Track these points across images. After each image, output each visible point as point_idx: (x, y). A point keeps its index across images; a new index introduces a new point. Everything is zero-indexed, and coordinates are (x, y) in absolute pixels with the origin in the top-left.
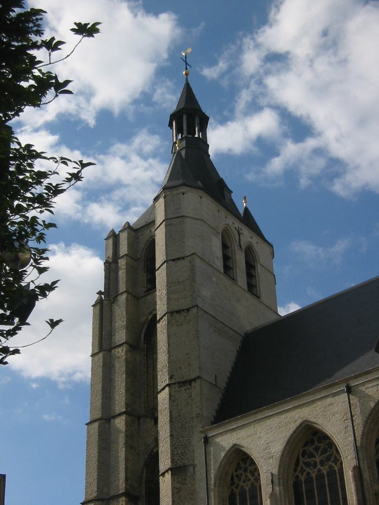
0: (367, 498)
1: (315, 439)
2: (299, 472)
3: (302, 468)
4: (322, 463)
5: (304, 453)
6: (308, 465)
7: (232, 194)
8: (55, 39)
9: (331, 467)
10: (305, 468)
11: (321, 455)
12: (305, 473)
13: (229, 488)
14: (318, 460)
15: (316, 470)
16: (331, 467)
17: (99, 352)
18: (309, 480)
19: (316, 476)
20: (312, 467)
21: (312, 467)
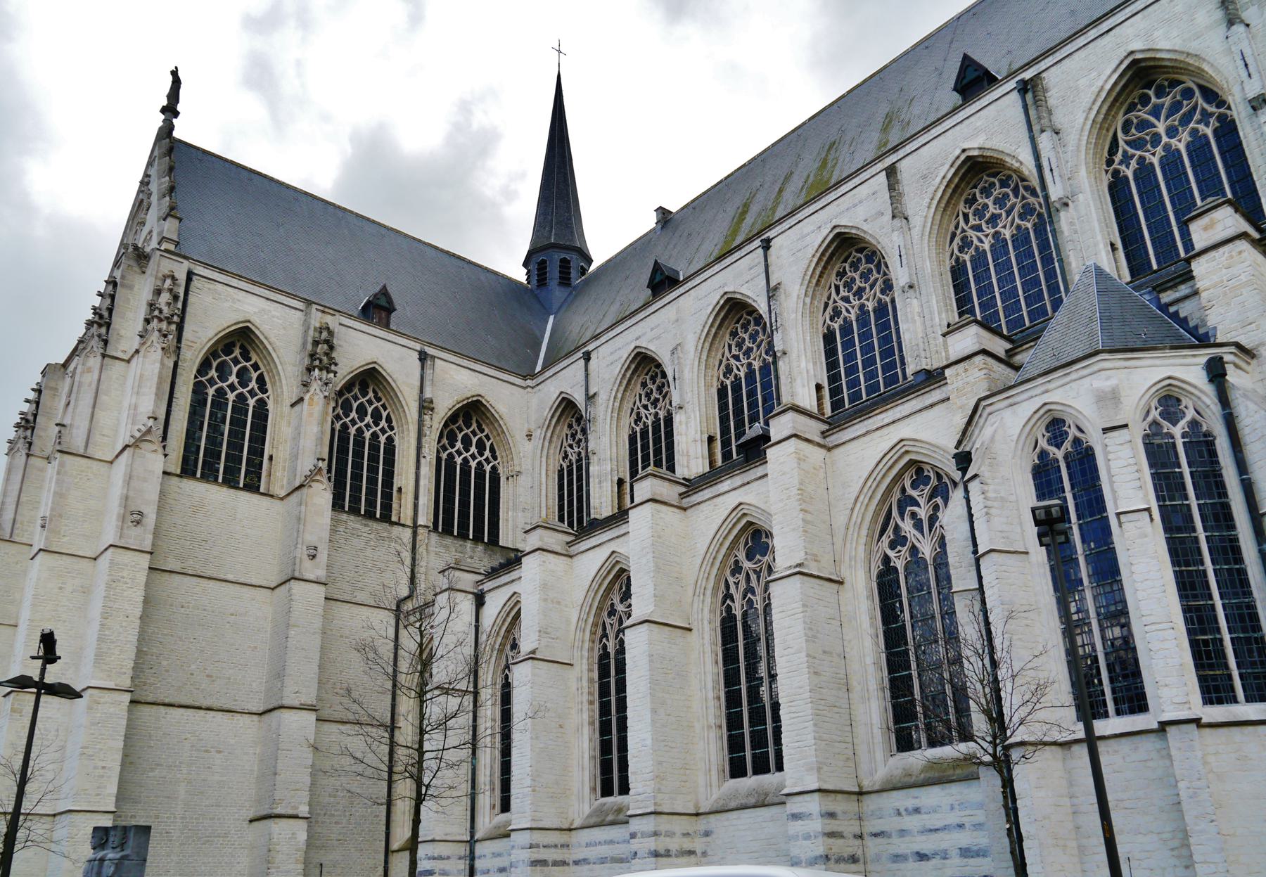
0: (972, 861)
1: (1151, 93)
2: (1121, 163)
3: (1125, 152)
4: (1172, 132)
5: (1126, 127)
6: (1137, 144)
7: (674, 207)
8: (561, 284)
9: (1194, 132)
10: (1131, 151)
11: (1167, 118)
12: (1133, 163)
13: (1107, 172)
14: (1161, 128)
15: (1159, 149)
16: (1194, 132)
17: (1242, 21)
18: (1145, 171)
19: (1188, 146)
20: (1149, 146)
21: (1149, 146)
